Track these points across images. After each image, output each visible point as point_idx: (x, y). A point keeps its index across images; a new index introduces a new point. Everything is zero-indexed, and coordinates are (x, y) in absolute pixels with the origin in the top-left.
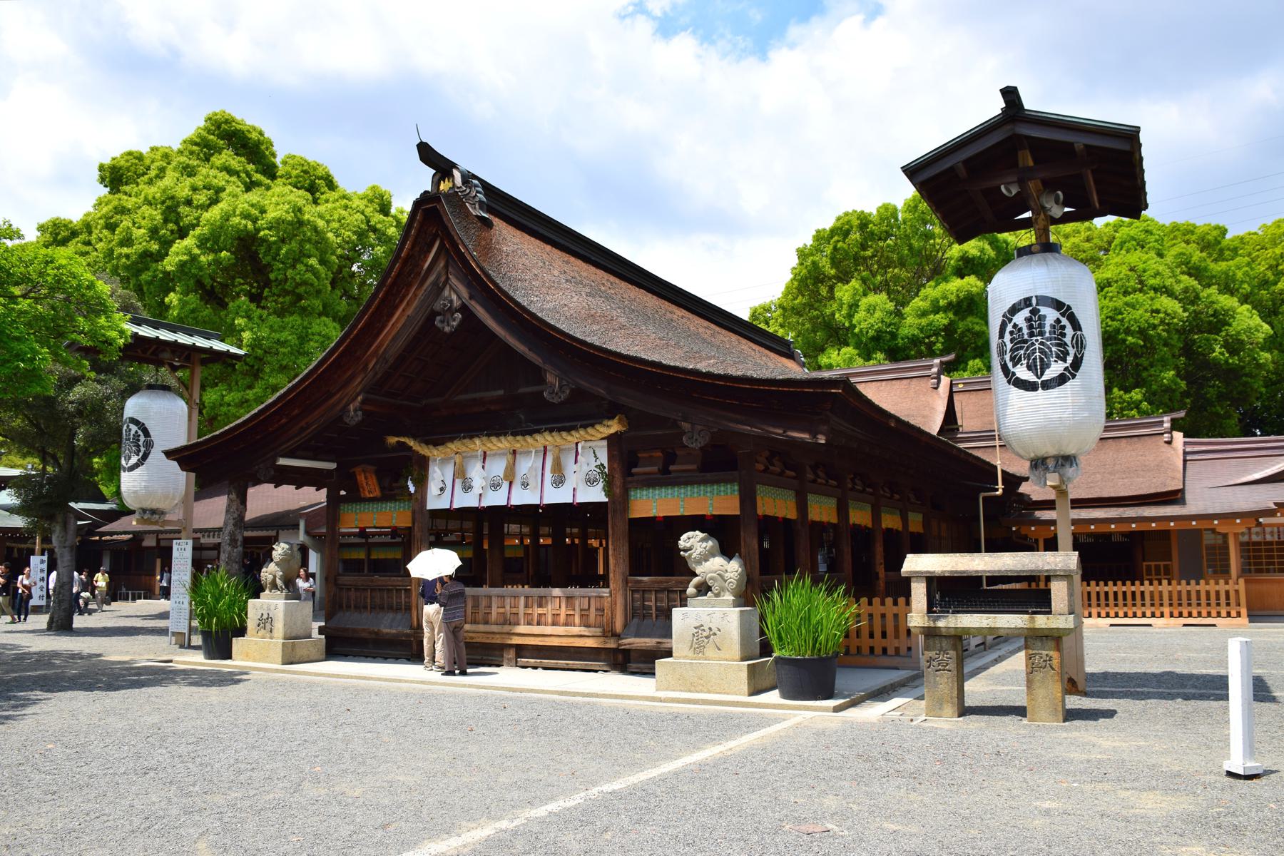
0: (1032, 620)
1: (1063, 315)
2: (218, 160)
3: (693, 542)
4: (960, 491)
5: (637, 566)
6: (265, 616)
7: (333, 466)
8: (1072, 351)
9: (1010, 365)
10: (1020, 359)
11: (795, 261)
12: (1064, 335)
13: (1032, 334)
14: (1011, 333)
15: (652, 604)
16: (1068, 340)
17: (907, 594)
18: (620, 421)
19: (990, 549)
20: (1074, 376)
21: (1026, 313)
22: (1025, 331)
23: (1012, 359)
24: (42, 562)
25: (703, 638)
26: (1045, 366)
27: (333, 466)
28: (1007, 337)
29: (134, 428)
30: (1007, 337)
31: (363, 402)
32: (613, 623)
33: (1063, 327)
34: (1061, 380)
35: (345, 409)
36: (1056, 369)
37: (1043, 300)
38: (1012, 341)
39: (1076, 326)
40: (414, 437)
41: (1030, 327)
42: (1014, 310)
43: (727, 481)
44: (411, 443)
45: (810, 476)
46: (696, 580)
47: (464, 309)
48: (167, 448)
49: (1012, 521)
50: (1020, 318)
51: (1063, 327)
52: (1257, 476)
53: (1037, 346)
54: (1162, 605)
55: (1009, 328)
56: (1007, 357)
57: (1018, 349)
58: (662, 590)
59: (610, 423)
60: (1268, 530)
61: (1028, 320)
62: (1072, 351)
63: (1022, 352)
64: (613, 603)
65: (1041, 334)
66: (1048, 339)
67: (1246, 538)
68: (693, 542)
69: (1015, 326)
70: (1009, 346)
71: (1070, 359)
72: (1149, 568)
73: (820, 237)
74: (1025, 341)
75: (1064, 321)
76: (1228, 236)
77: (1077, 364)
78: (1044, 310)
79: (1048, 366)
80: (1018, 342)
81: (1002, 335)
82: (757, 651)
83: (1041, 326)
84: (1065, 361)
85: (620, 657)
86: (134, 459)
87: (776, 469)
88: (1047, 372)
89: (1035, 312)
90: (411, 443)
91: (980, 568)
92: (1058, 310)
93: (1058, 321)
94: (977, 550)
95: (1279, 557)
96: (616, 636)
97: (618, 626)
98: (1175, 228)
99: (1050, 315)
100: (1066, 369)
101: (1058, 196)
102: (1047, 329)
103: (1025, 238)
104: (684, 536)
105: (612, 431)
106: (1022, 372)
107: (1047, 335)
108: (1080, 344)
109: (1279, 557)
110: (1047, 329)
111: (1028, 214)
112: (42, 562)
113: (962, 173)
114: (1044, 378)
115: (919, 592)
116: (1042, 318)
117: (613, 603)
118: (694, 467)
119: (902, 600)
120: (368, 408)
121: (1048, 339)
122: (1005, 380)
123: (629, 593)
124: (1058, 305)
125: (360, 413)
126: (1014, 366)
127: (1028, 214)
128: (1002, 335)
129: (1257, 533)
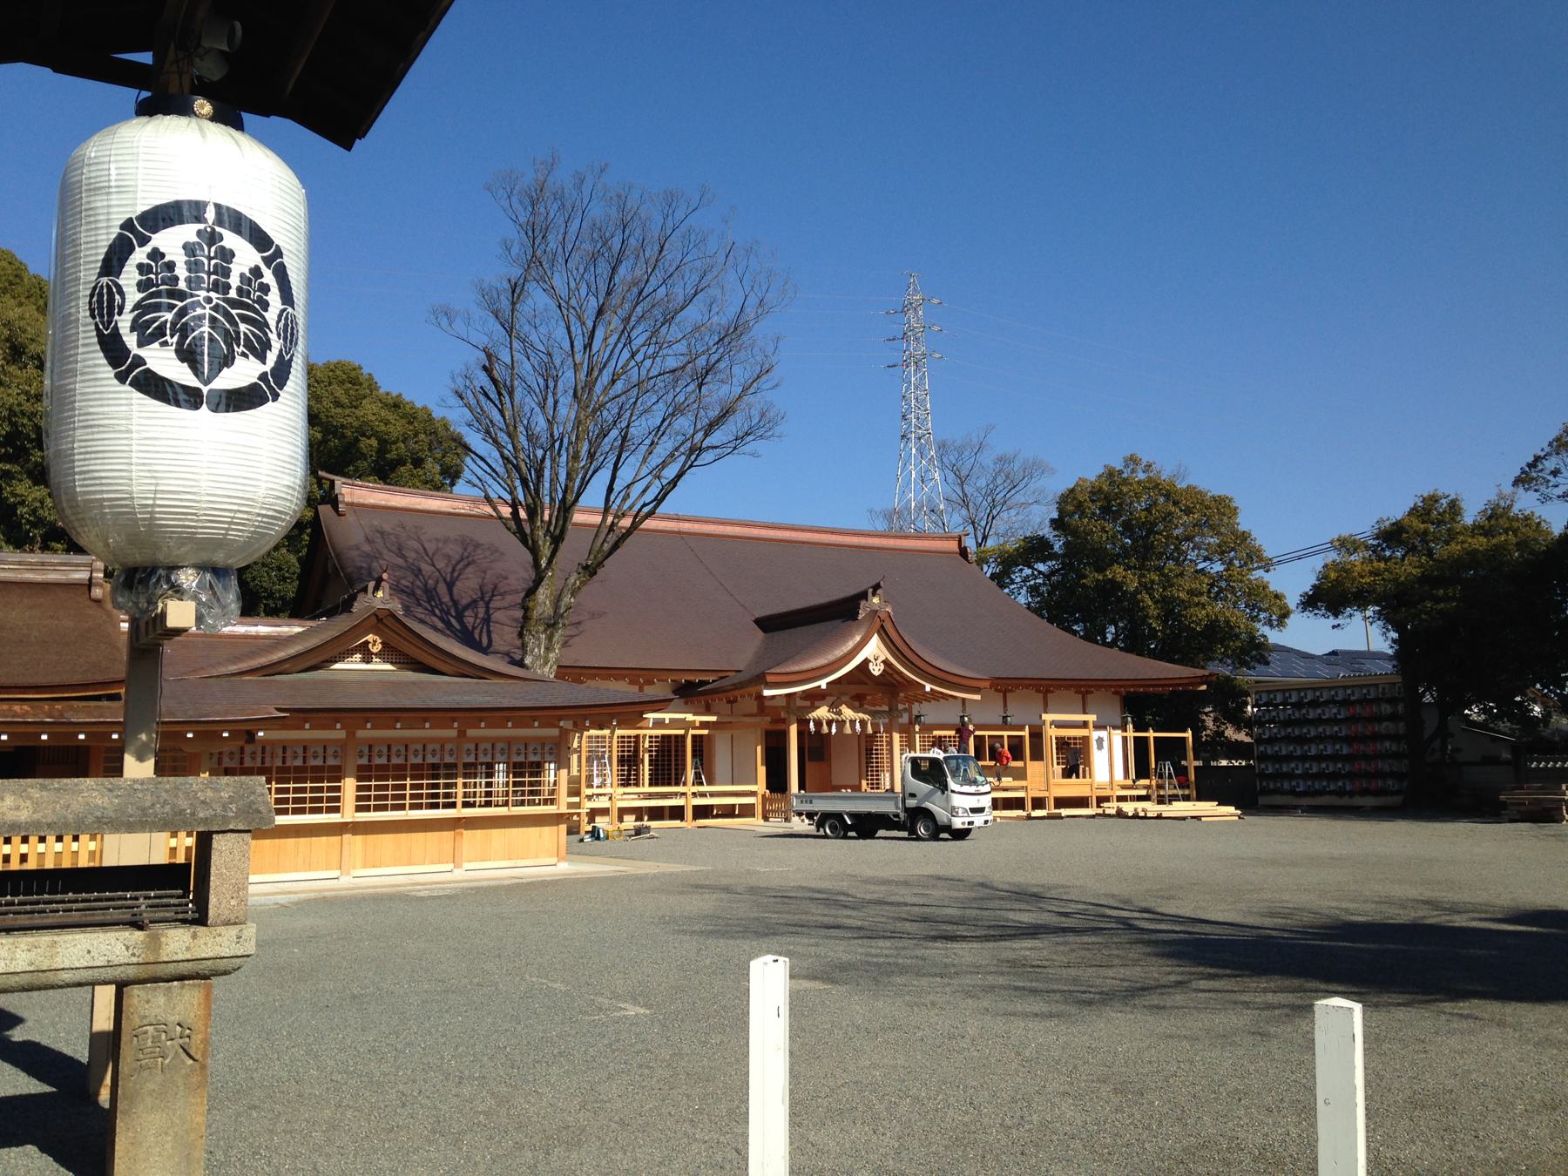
0: (155, 943)
6: (489, 588)
8: (277, 345)
10: (160, 332)
12: (265, 305)
16: (271, 316)
33: (265, 289)
36: (243, 372)
41: (193, 266)
51: (265, 289)
52: (233, 668)
53: (208, 311)
55: (140, 255)
56: (124, 322)
57: (157, 307)
61: (189, 249)
62: (277, 345)
63: (169, 316)
66: (234, 304)
69: (156, 255)
70: (133, 296)
71: (272, 357)
74: (181, 296)
75: (269, 277)
79: (228, 361)
89: (213, 238)
92: (260, 250)
93: (256, 272)
100: (263, 377)
101: (233, 29)
102: (234, 281)
104: (215, 79)
107: (233, 294)
110: (234, 281)
111: (146, 58)
121: (234, 304)
127: (146, 58)
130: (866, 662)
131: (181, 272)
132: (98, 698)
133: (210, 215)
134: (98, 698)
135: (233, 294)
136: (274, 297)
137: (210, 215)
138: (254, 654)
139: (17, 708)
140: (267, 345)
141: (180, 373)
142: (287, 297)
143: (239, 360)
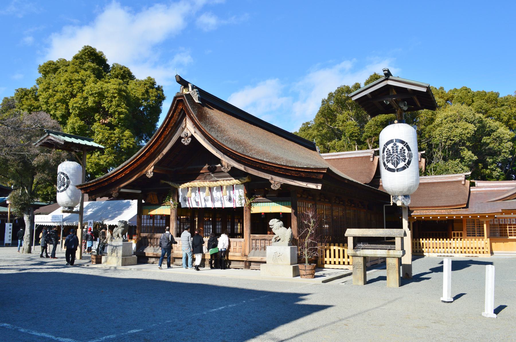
0: (389, 252)
1: (404, 146)
2: (86, 66)
3: (274, 223)
4: (371, 205)
5: (254, 231)
7: (140, 192)
8: (407, 159)
9: (386, 162)
11: (321, 104)
12: (404, 153)
13: (393, 152)
14: (387, 152)
15: (259, 244)
16: (406, 154)
17: (347, 242)
18: (248, 178)
19: (387, 227)
20: (408, 167)
21: (392, 144)
22: (391, 151)
23: (387, 161)
24: (10, 225)
25: (278, 256)
26: (398, 164)
27: (140, 192)
28: (385, 153)
29: (62, 176)
30: (385, 153)
31: (153, 170)
32: (245, 251)
33: (404, 150)
34: (404, 168)
35: (147, 172)
36: (402, 164)
37: (397, 140)
38: (387, 154)
39: (409, 149)
40: (172, 181)
41: (393, 150)
42: (388, 143)
43: (288, 201)
44: (170, 184)
45: (318, 198)
46: (275, 236)
47: (192, 137)
48: (506, 308)
49: (392, 216)
50: (390, 147)
51: (404, 150)
52: (494, 199)
54: (430, 248)
55: (386, 150)
56: (385, 160)
58: (263, 240)
59: (245, 178)
60: (501, 220)
61: (393, 147)
64: (245, 244)
65: (397, 152)
67: (492, 223)
68: (274, 223)
69: (388, 149)
70: (386, 156)
71: (407, 161)
72: (454, 234)
73: (331, 95)
74: (391, 155)
75: (405, 148)
76: (500, 96)
77: (409, 163)
78: (398, 144)
80: (389, 155)
81: (383, 152)
82: (297, 262)
83: (397, 149)
84: (405, 162)
85: (248, 264)
86: (62, 188)
87: (305, 196)
88: (399, 165)
89: (395, 144)
90: (170, 184)
91: (371, 234)
93: (403, 148)
94: (382, 227)
95: (514, 230)
96: (245, 255)
97: (247, 253)
98: (479, 93)
99: (400, 146)
100: (405, 165)
102: (399, 150)
103: (305, 196)
104: (271, 221)
105: (245, 181)
106: (390, 165)
107: (399, 153)
108: (410, 156)
109: (514, 230)
110: (399, 150)
112: (10, 225)
113: (370, 97)
114: (398, 167)
115: (350, 241)
116: (397, 147)
117: (245, 244)
118: (275, 195)
119: (345, 244)
120: (155, 171)
122: (384, 168)
123: (251, 241)
124: (402, 142)
125: (152, 173)
126: (388, 163)
128: (383, 152)
129: (496, 221)
130: (180, 138)
131: (391, 151)
132: (460, 208)
133: (394, 141)
134: (460, 208)
135: (399, 153)
136: (406, 151)
137: (394, 141)
138: (505, 193)
139: (442, 211)
140: (405, 159)
141: (392, 167)
142: (409, 149)
143: (401, 163)
